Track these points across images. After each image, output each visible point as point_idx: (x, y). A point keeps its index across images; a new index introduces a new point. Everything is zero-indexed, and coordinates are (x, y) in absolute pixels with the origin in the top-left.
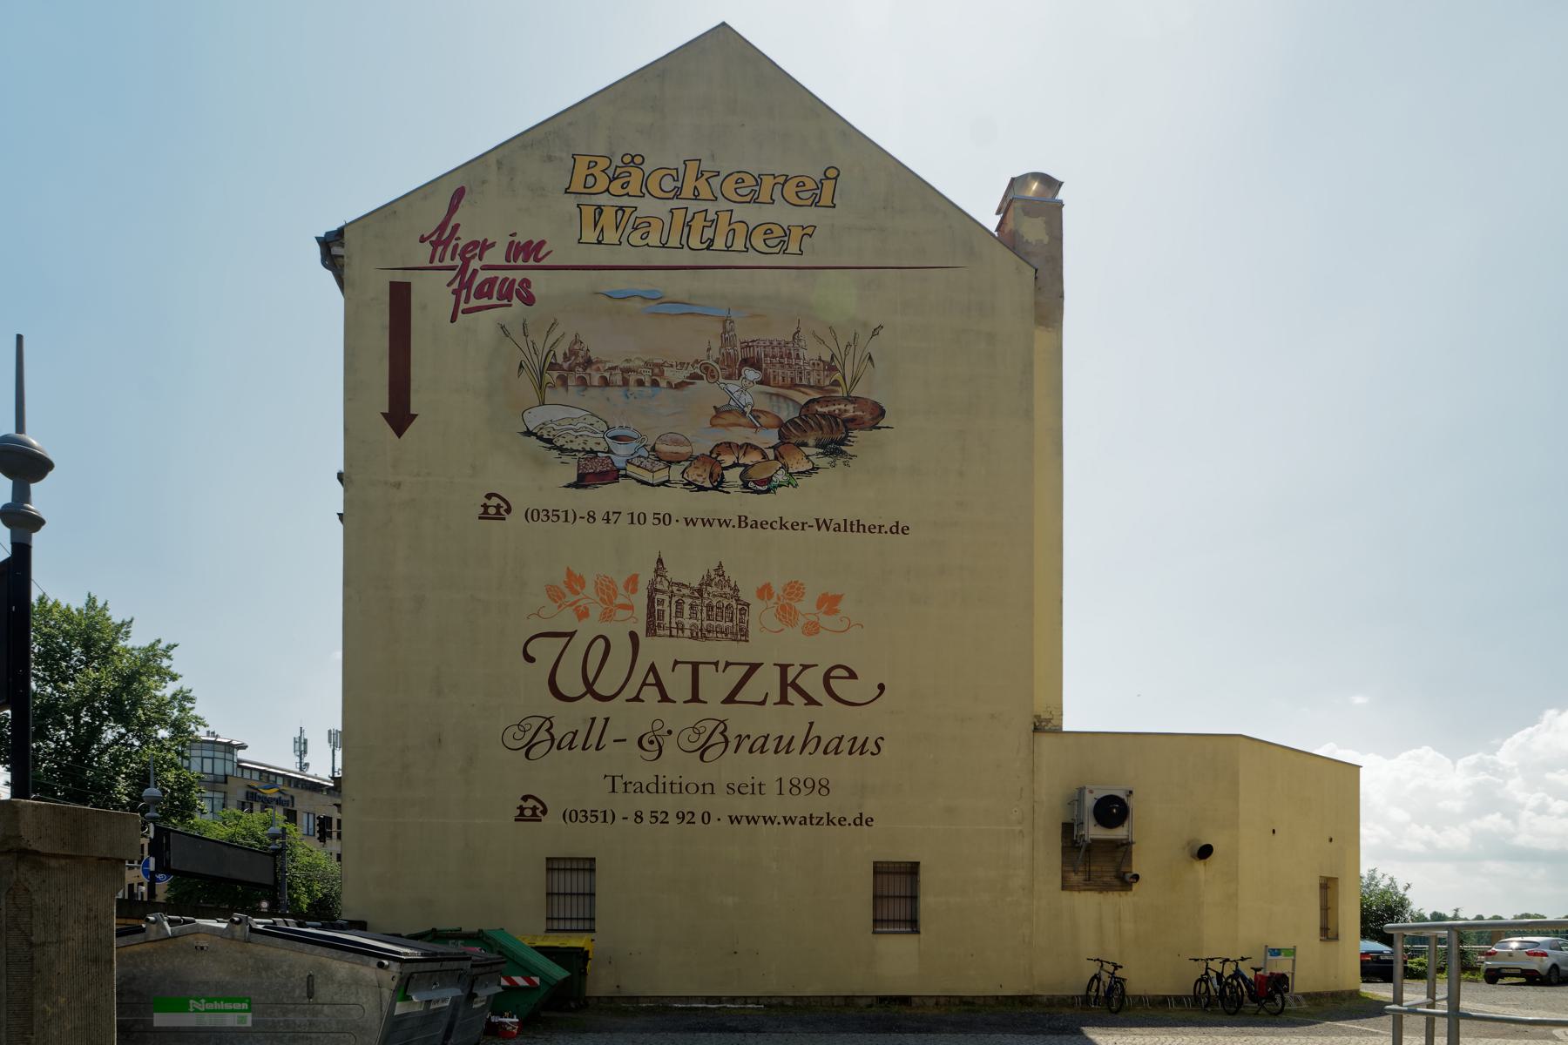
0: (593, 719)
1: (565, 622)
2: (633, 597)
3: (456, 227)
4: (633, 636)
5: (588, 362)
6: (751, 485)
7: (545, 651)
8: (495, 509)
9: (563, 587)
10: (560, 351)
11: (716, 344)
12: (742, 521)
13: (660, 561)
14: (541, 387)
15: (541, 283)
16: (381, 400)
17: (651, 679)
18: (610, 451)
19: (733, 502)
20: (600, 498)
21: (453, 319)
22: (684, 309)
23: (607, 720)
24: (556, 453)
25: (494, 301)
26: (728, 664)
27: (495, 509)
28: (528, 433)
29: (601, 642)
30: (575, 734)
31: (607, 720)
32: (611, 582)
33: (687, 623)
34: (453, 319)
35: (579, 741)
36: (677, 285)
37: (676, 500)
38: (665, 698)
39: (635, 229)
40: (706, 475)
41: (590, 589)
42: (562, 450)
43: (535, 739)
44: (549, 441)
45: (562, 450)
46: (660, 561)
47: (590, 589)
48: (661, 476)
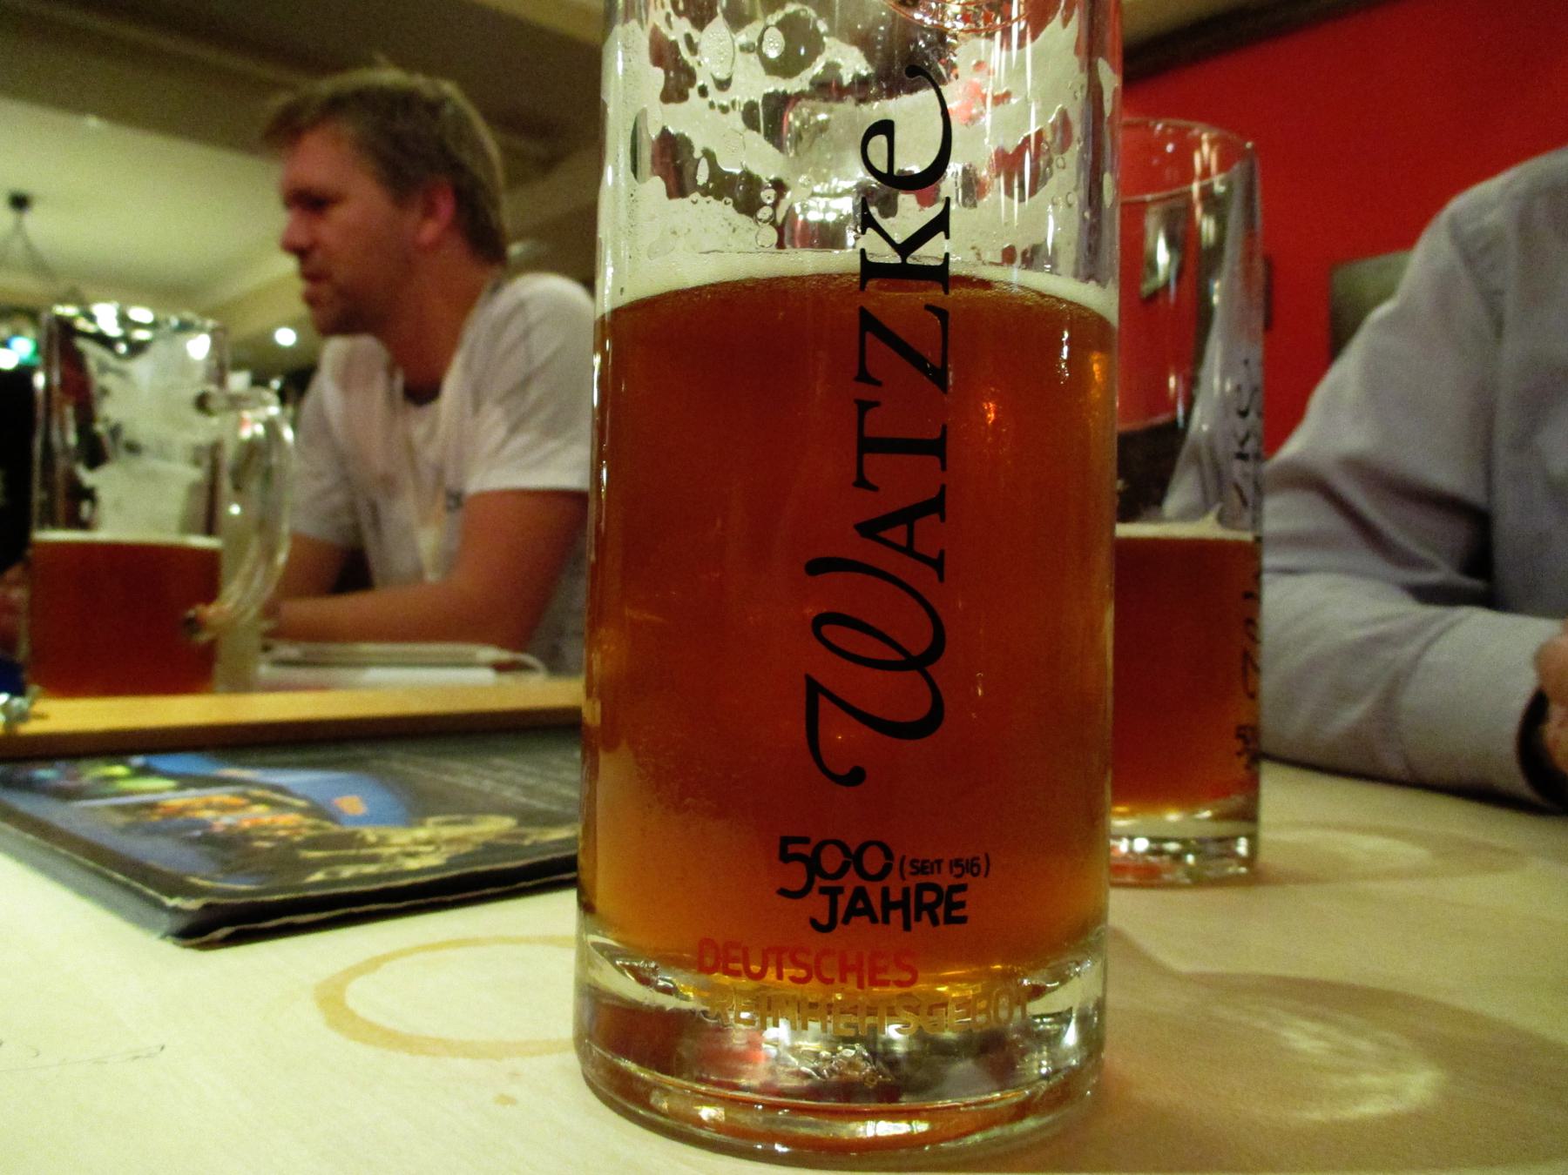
17: (898, 534)
29: (828, 631)
38: (936, 505)
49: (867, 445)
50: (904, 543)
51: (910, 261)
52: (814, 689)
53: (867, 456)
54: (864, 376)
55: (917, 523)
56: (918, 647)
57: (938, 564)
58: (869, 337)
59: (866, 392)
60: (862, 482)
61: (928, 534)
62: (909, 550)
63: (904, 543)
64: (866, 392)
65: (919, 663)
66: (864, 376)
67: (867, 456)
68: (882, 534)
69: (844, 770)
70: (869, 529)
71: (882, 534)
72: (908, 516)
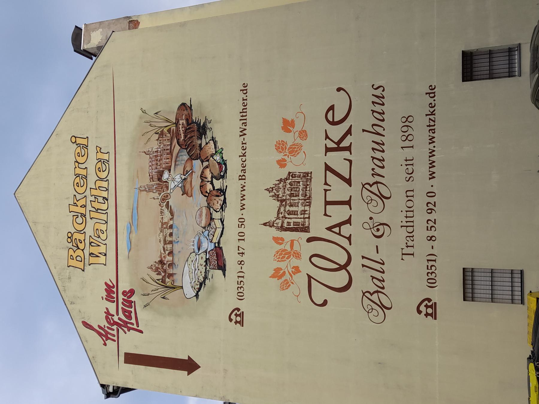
1: (301, 280)
3: (99, 326)
6: (222, 174)
17: (336, 230)
18: (206, 252)
21: (141, 332)
27: (238, 317)
29: (314, 259)
30: (373, 278)
32: (277, 252)
33: (301, 208)
37: (231, 215)
38: (348, 221)
39: (99, 237)
42: (205, 278)
48: (218, 223)
49: (327, 203)
50: (338, 232)
51: (340, 146)
52: (310, 277)
53: (327, 206)
54: (326, 184)
55: (342, 227)
56: (343, 262)
57: (349, 239)
58: (348, 177)
59: (327, 187)
60: (402, 259)
61: (346, 230)
62: (339, 234)
63: (338, 232)
64: (327, 187)
65: (344, 267)
66: (326, 184)
67: (327, 206)
68: (333, 230)
69: (321, 302)
70: (330, 229)
71: (333, 230)
72: (339, 225)
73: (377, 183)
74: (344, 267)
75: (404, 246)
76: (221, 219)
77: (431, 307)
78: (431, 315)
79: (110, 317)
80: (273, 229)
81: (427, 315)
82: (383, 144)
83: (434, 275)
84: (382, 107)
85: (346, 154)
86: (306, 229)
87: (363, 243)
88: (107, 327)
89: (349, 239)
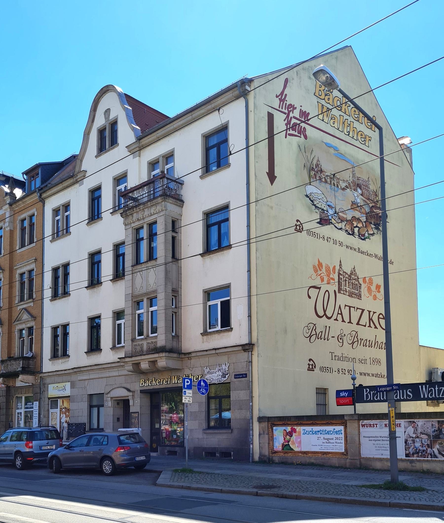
0: (326, 326)
1: (317, 282)
2: (334, 275)
3: (286, 95)
4: (335, 291)
5: (321, 171)
6: (360, 236)
7: (314, 292)
8: (299, 228)
9: (317, 266)
10: (315, 162)
11: (351, 176)
12: (359, 251)
13: (340, 261)
14: (310, 177)
15: (310, 131)
16: (176, 241)
17: (340, 312)
18: (327, 211)
19: (355, 241)
20: (326, 230)
21: (286, 137)
22: (341, 156)
23: (329, 327)
24: (314, 207)
25: (296, 133)
26: (357, 308)
27: (299, 228)
28: (307, 196)
29: (327, 292)
30: (322, 332)
31: (329, 327)
32: (329, 267)
33: (348, 289)
34: (286, 137)
35: (323, 336)
36: (343, 148)
37: (342, 236)
38: (343, 321)
39: (332, 119)
40: (350, 228)
41: (324, 270)
42: (316, 207)
43: (313, 334)
44: (312, 201)
45: (316, 207)
46: (340, 261)
47: (324, 270)
48: (339, 226)
73: (358, 341)
74: (325, 314)
75: (335, 354)
76: (342, 228)
77: (312, 368)
78: (309, 368)
79: (292, 109)
80: (339, 268)
81: (309, 365)
82: (328, 340)
83: (325, 371)
84: (323, 339)
85: (368, 325)
86: (340, 290)
87: (336, 327)
88: (286, 104)
89: (336, 320)
